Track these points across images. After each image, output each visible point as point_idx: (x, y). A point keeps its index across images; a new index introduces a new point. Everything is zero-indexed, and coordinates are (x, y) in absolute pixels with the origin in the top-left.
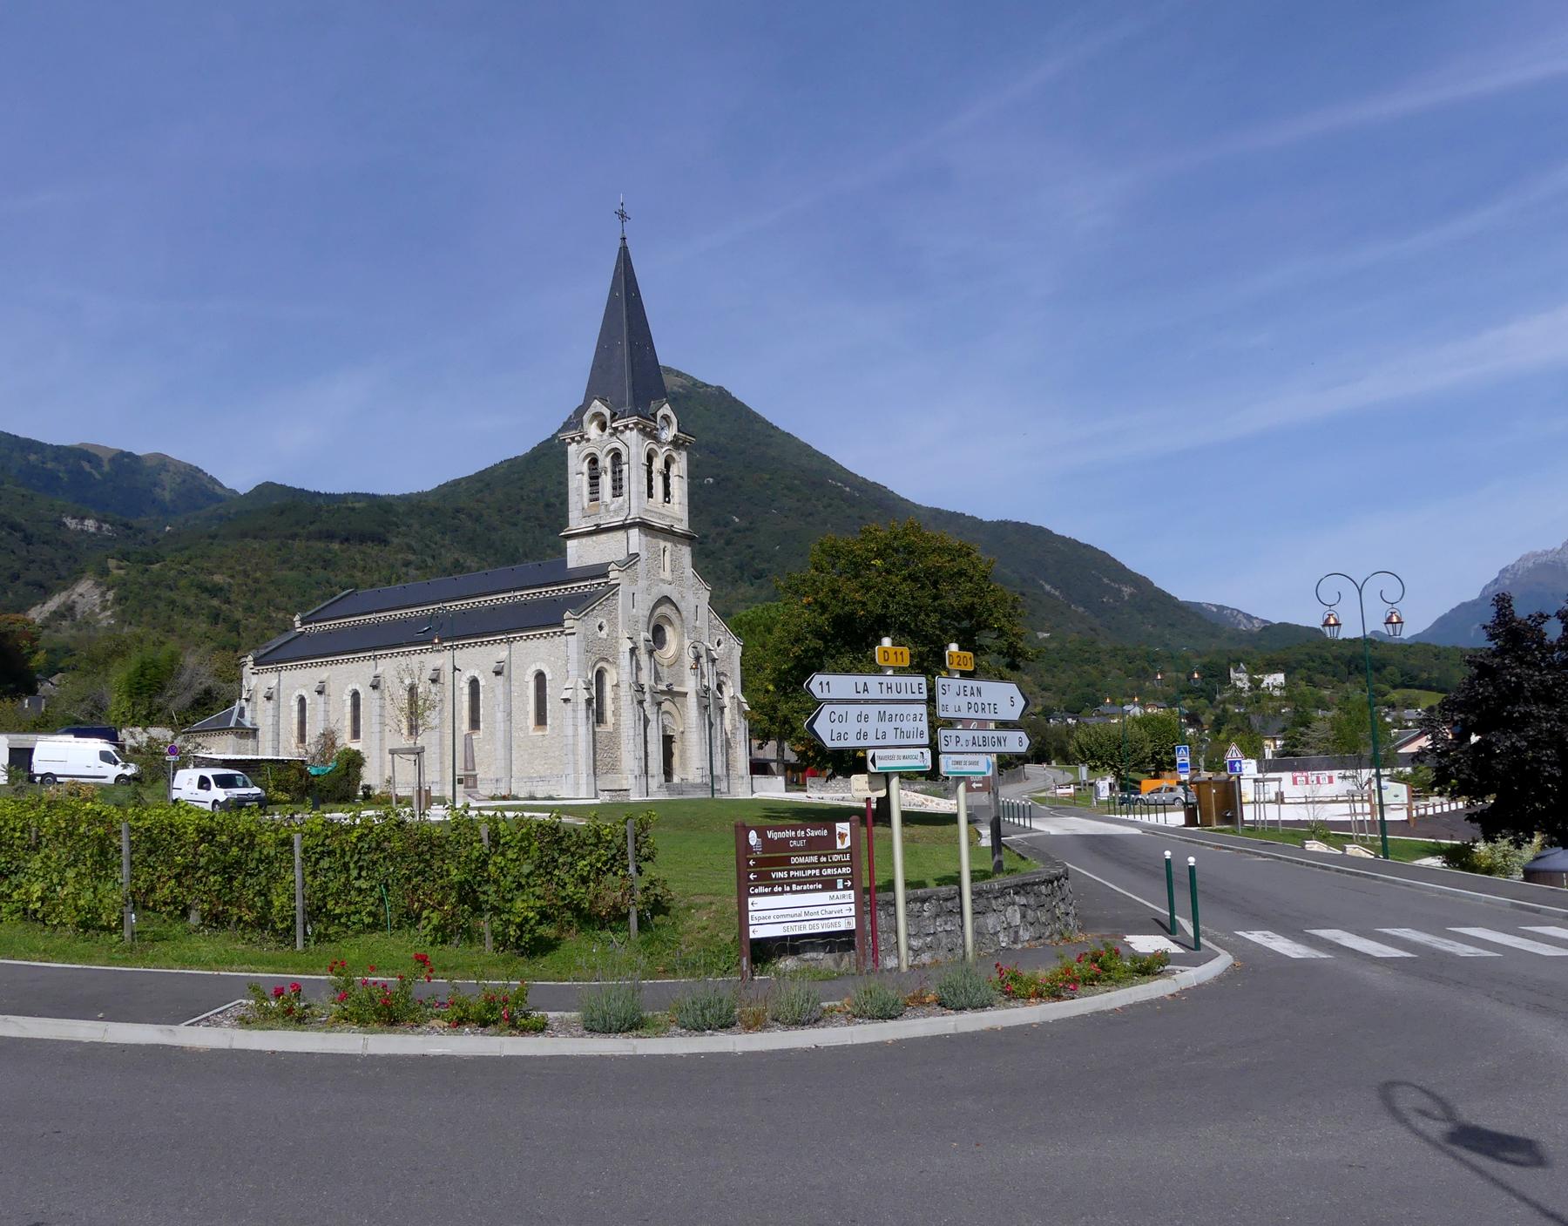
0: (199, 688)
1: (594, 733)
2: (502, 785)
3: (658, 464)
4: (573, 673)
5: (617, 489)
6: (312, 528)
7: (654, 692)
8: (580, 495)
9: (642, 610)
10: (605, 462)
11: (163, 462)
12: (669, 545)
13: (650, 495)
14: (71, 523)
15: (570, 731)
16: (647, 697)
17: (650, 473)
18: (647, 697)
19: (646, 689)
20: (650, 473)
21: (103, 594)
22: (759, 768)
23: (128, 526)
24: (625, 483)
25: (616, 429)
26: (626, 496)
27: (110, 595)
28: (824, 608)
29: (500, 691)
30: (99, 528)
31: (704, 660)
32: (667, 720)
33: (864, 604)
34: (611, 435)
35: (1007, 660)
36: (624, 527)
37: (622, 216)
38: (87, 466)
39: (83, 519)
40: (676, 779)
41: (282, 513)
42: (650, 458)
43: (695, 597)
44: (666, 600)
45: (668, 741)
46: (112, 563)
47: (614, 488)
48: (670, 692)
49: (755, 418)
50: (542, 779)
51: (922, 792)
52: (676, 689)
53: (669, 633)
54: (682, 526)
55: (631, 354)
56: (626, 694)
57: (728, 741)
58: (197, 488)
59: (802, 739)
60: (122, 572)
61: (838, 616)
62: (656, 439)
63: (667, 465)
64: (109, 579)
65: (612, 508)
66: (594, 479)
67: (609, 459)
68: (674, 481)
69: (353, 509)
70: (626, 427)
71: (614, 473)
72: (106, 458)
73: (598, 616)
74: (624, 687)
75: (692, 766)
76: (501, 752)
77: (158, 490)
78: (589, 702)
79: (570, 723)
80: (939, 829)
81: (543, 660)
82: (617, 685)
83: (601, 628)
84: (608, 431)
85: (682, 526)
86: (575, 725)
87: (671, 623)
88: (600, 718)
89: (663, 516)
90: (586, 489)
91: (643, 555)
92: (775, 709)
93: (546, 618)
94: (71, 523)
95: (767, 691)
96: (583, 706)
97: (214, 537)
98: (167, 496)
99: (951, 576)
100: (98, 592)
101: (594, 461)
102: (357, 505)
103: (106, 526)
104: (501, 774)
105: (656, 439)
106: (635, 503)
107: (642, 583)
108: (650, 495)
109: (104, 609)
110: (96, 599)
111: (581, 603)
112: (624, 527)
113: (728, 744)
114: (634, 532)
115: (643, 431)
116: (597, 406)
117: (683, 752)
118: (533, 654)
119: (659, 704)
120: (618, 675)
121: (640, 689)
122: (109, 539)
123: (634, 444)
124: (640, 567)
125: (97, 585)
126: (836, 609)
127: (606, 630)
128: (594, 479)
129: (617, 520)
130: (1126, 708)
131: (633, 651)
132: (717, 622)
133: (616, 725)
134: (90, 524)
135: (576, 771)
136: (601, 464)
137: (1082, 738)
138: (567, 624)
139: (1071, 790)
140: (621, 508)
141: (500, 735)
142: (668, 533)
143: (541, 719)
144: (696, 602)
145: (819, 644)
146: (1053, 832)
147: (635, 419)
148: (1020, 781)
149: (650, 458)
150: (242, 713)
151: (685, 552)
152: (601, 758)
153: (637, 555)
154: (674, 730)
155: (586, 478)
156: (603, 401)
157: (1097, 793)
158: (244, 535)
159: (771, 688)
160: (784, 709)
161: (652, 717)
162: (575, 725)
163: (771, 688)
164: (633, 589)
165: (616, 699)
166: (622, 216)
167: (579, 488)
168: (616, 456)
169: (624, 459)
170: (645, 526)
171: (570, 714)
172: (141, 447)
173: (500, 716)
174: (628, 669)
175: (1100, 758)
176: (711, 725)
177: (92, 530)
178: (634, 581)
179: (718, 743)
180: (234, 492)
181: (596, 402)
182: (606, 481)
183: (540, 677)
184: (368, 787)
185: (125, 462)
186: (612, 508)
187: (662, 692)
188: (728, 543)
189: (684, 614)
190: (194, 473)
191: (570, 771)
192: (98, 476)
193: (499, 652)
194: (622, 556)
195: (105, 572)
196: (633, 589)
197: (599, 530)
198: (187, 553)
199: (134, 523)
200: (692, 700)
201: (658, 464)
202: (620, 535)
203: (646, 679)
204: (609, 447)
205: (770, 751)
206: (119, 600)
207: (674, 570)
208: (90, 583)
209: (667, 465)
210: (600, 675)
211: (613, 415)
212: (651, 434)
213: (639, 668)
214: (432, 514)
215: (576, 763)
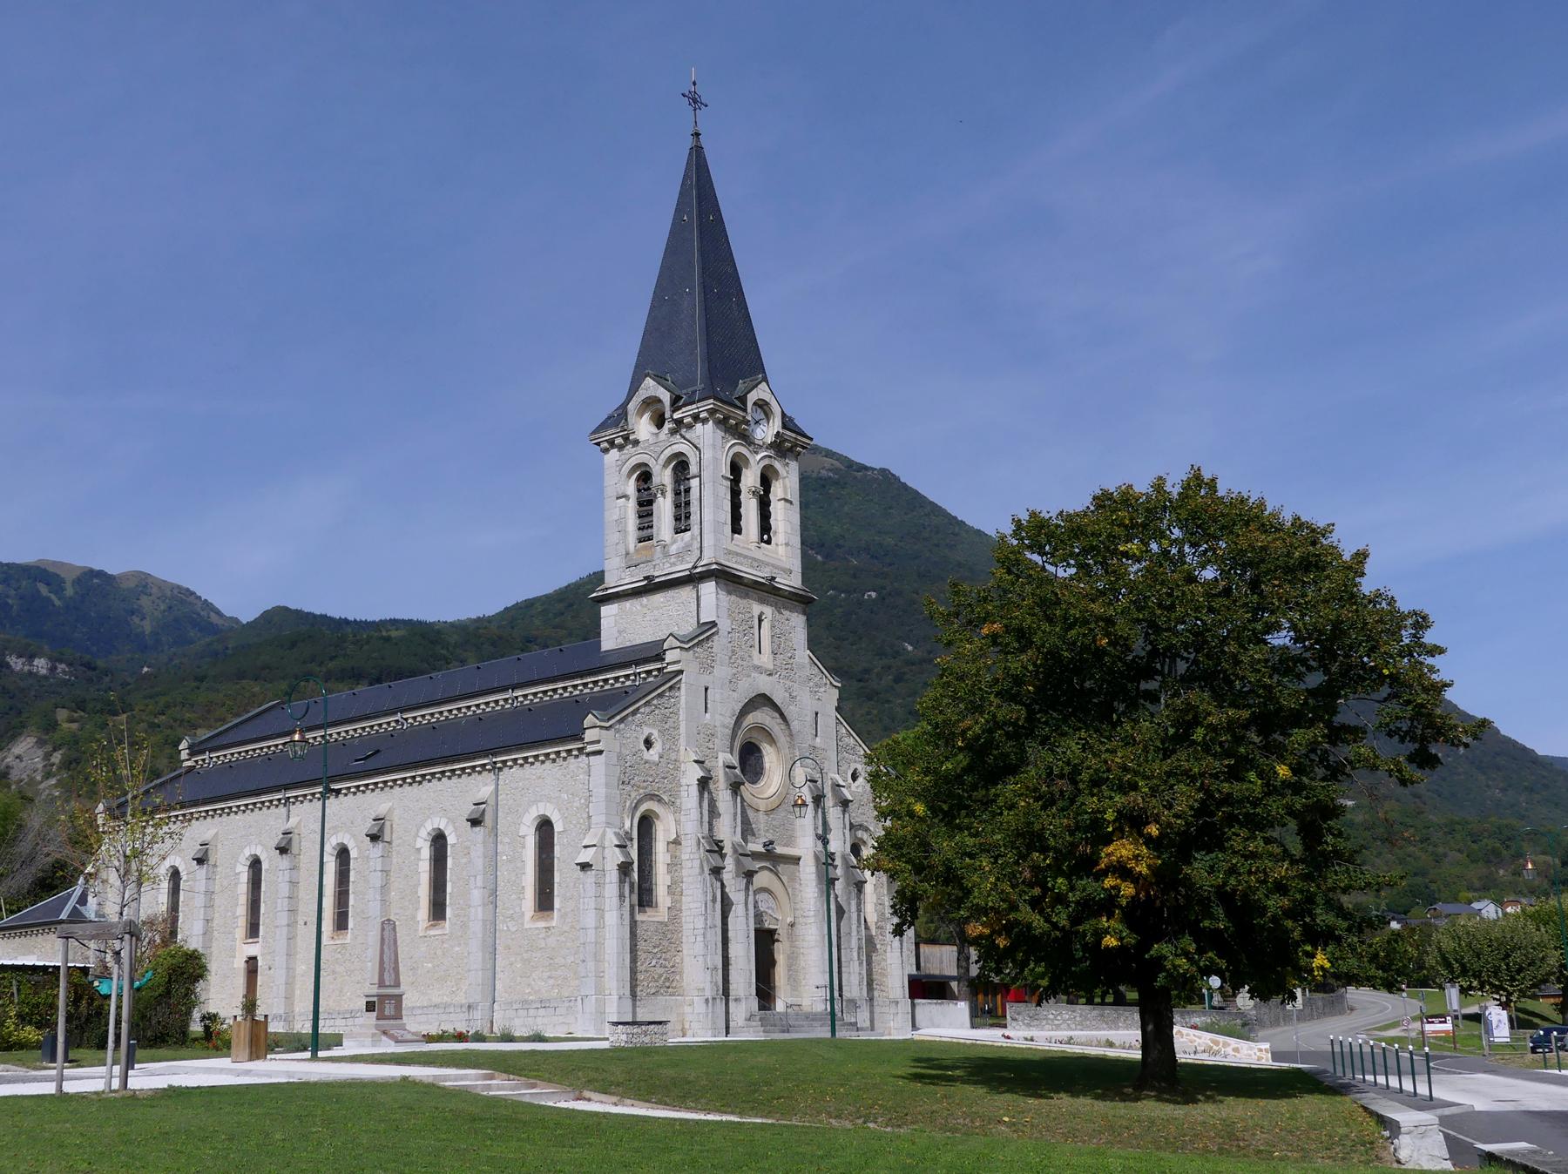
0: (43, 861)
1: (634, 924)
2: (477, 1014)
3: (750, 479)
4: (599, 819)
5: (682, 520)
6: (331, 665)
7: (741, 855)
8: (623, 532)
9: (722, 715)
10: (663, 476)
11: (144, 583)
12: (768, 611)
13: (736, 528)
14: (17, 663)
15: (590, 920)
16: (729, 863)
17: (735, 494)
18: (729, 863)
19: (728, 850)
20: (735, 494)
21: (47, 756)
22: (925, 988)
23: (90, 666)
24: (694, 508)
25: (679, 422)
26: (695, 529)
27: (57, 758)
28: (1024, 637)
29: (478, 853)
30: (53, 669)
31: (829, 801)
32: (765, 903)
33: (1109, 621)
34: (673, 432)
35: (1413, 747)
36: (692, 579)
37: (695, 101)
38: (43, 590)
39: (31, 657)
40: (780, 1006)
41: (293, 645)
42: (736, 469)
43: (813, 698)
44: (762, 700)
45: (765, 940)
46: (62, 714)
47: (677, 519)
48: (770, 857)
49: (936, 509)
50: (544, 1004)
51: (1208, 1029)
52: (779, 850)
53: (771, 758)
54: (792, 581)
55: (706, 309)
56: (692, 858)
57: (870, 941)
58: (187, 614)
59: (984, 911)
60: (74, 726)
61: (1053, 654)
62: (746, 438)
63: (766, 481)
64: (56, 736)
65: (673, 549)
66: (645, 506)
67: (668, 472)
68: (778, 510)
69: (388, 639)
70: (696, 418)
71: (677, 493)
72: (69, 578)
73: (644, 724)
74: (689, 845)
75: (804, 985)
76: (476, 958)
77: (136, 620)
78: (624, 869)
79: (594, 904)
80: (1282, 1106)
81: (549, 799)
82: (677, 842)
83: (648, 743)
84: (668, 426)
85: (792, 581)
86: (600, 910)
87: (772, 741)
88: (645, 897)
89: (759, 563)
90: (632, 522)
91: (724, 625)
92: (925, 846)
93: (556, 731)
94: (17, 663)
95: (911, 814)
96: (613, 876)
97: (201, 679)
98: (147, 627)
99: (1288, 570)
100: (40, 753)
101: (645, 476)
102: (394, 634)
103: (61, 667)
104: (476, 997)
105: (746, 438)
106: (712, 540)
107: (722, 671)
108: (736, 528)
109: (47, 776)
110: (38, 762)
111: (615, 705)
112: (692, 579)
113: (870, 945)
114: (709, 588)
115: (723, 423)
116: (650, 387)
117: (793, 958)
118: (533, 788)
119: (749, 875)
120: (679, 825)
121: (717, 848)
122: (65, 683)
123: (709, 446)
124: (719, 644)
125: (41, 743)
126: (1048, 635)
127: (657, 747)
128: (645, 506)
129: (682, 568)
130: (1476, 905)
131: (704, 783)
132: (851, 740)
133: (674, 910)
134: (41, 665)
135: (600, 990)
136: (656, 480)
137: (1448, 944)
138: (589, 735)
139: (1448, 1026)
140: (687, 549)
141: (476, 927)
142: (766, 590)
143: (545, 901)
144: (817, 706)
145: (1017, 712)
146: (1480, 1106)
147: (709, 404)
148: (1342, 1013)
149: (736, 469)
150: (83, 900)
151: (797, 624)
152: (645, 963)
153: (714, 624)
154: (777, 919)
155: (631, 506)
156: (660, 379)
157: (1489, 1031)
158: (241, 676)
159: (919, 808)
160: (945, 847)
161: (736, 896)
162: (600, 910)
163: (919, 808)
164: (706, 679)
165: (673, 866)
166: (695, 101)
167: (622, 520)
168: (681, 466)
169: (693, 469)
170: (726, 577)
171: (591, 890)
172: (115, 559)
173: (477, 895)
174: (695, 814)
175: (1477, 975)
176: (841, 912)
177: (44, 672)
178: (708, 667)
179: (853, 943)
180: (236, 620)
181: (649, 382)
182: (664, 508)
183: (545, 827)
184: (211, 1018)
185: (95, 582)
186: (673, 549)
187: (755, 856)
188: (898, 680)
189: (795, 725)
190: (184, 597)
191: (589, 989)
192: (57, 603)
193: (480, 787)
194: (688, 627)
195: (51, 726)
196: (706, 679)
197: (652, 587)
198: (162, 700)
199: (100, 663)
200: (808, 871)
201: (750, 479)
202: (686, 593)
203: (727, 830)
204: (668, 452)
205: (942, 960)
206: (67, 764)
207: (779, 656)
208: (31, 741)
209: (766, 481)
210: (646, 824)
211: (676, 403)
212: (739, 432)
213: (713, 812)
214: (493, 644)
215: (599, 976)
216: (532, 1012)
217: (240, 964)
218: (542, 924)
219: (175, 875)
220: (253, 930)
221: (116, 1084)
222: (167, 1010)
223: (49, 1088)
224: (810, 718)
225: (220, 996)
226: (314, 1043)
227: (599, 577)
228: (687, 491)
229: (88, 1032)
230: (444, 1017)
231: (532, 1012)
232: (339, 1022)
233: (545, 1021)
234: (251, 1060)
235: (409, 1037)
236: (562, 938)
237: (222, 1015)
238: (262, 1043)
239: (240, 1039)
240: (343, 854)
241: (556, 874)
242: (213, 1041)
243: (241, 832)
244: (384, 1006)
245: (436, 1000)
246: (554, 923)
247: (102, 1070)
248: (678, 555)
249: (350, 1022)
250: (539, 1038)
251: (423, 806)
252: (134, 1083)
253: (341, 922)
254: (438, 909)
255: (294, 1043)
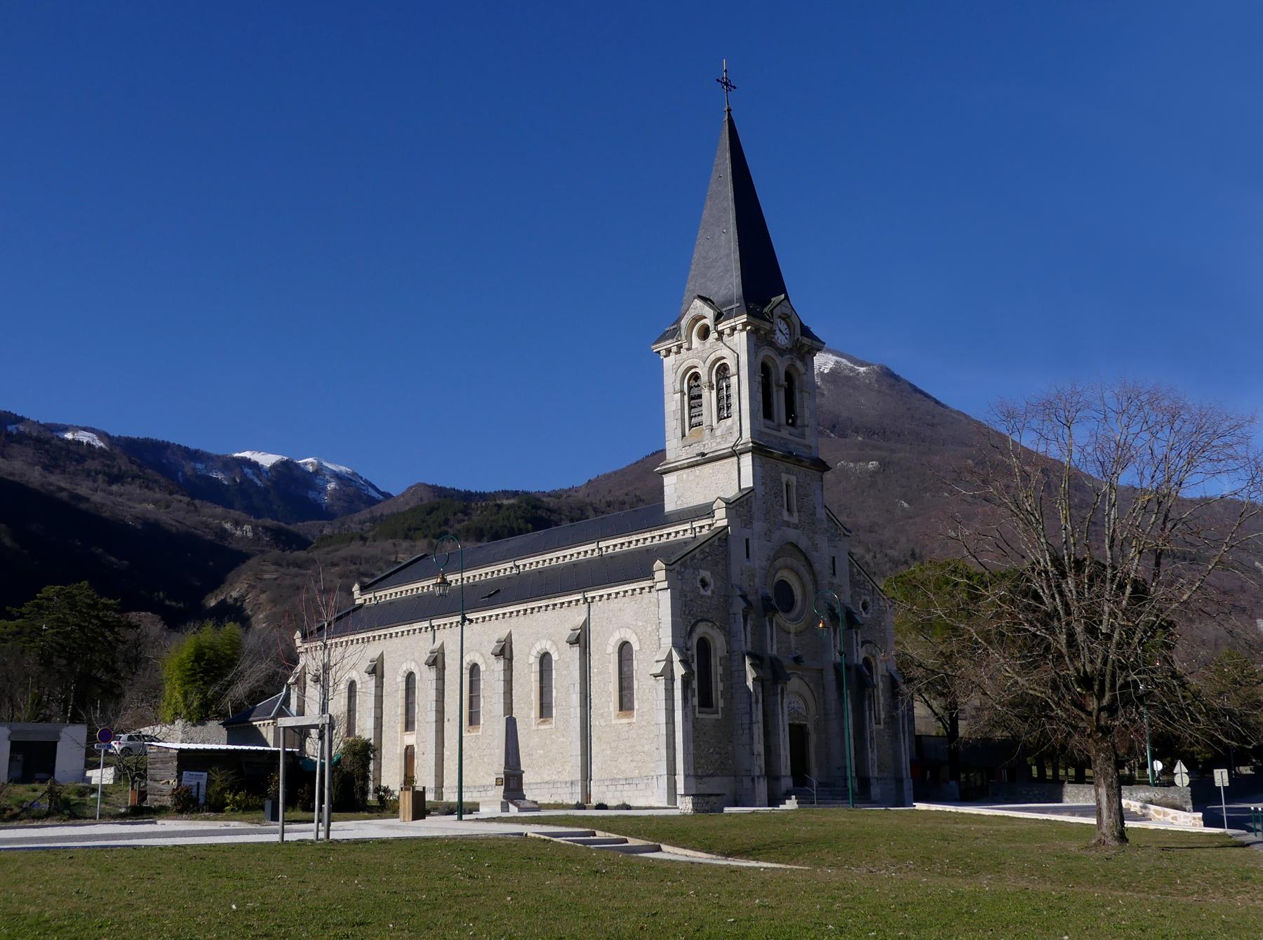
24: (734, 400)
26: (735, 416)
47: (719, 409)
50: (628, 781)
102: (506, 502)
147: (744, 318)
182: (709, 398)
197: (705, 459)
211: (718, 318)
216: (619, 788)
217: (400, 751)
218: (625, 721)
219: (352, 685)
220: (409, 725)
221: (322, 835)
222: (353, 787)
223: (275, 838)
224: (828, 562)
225: (390, 776)
226: (460, 809)
227: (662, 453)
228: (728, 387)
229: (300, 796)
230: (554, 791)
231: (619, 788)
232: (475, 794)
233: (630, 794)
234: (414, 819)
235: (528, 805)
236: (641, 731)
237: (391, 788)
238: (421, 810)
239: (406, 802)
240: (474, 668)
241: (635, 682)
242: (385, 807)
243: (405, 649)
244: (512, 784)
245: (547, 778)
246: (634, 720)
247: (313, 826)
248: (722, 436)
249: (483, 794)
250: (628, 808)
251: (541, 628)
252: (333, 836)
253: (474, 720)
254: (748, 556)
255: (449, 810)
